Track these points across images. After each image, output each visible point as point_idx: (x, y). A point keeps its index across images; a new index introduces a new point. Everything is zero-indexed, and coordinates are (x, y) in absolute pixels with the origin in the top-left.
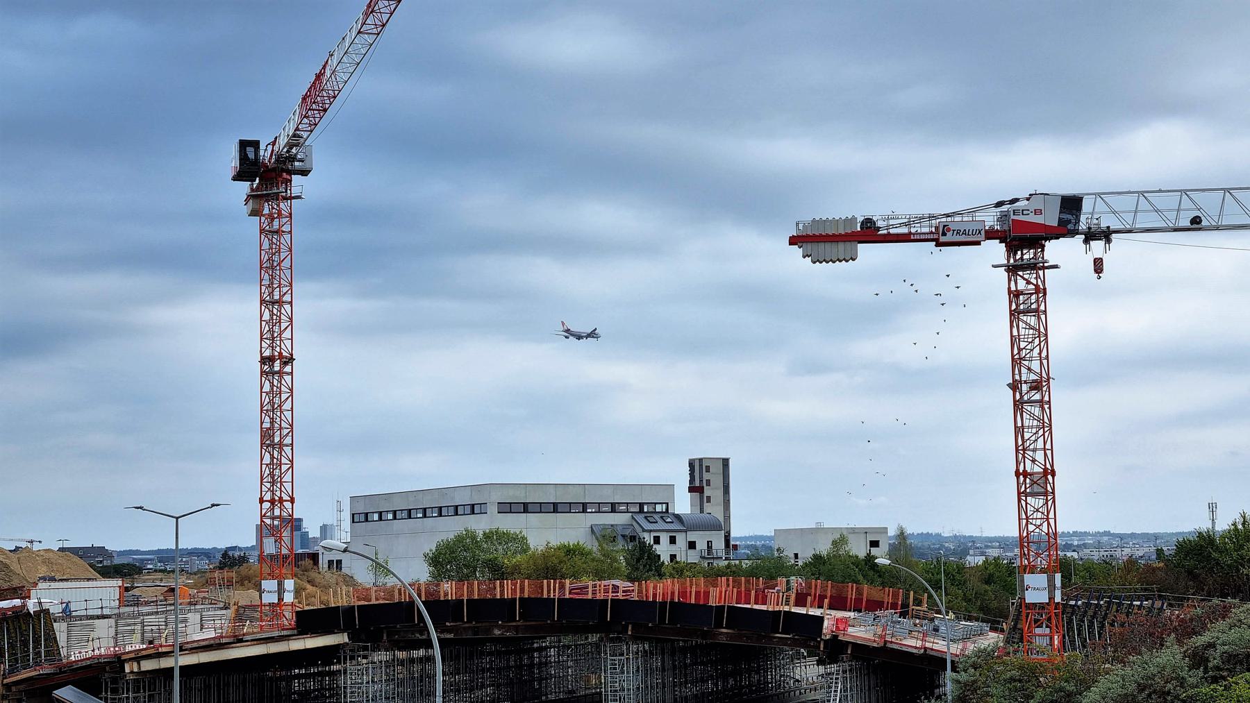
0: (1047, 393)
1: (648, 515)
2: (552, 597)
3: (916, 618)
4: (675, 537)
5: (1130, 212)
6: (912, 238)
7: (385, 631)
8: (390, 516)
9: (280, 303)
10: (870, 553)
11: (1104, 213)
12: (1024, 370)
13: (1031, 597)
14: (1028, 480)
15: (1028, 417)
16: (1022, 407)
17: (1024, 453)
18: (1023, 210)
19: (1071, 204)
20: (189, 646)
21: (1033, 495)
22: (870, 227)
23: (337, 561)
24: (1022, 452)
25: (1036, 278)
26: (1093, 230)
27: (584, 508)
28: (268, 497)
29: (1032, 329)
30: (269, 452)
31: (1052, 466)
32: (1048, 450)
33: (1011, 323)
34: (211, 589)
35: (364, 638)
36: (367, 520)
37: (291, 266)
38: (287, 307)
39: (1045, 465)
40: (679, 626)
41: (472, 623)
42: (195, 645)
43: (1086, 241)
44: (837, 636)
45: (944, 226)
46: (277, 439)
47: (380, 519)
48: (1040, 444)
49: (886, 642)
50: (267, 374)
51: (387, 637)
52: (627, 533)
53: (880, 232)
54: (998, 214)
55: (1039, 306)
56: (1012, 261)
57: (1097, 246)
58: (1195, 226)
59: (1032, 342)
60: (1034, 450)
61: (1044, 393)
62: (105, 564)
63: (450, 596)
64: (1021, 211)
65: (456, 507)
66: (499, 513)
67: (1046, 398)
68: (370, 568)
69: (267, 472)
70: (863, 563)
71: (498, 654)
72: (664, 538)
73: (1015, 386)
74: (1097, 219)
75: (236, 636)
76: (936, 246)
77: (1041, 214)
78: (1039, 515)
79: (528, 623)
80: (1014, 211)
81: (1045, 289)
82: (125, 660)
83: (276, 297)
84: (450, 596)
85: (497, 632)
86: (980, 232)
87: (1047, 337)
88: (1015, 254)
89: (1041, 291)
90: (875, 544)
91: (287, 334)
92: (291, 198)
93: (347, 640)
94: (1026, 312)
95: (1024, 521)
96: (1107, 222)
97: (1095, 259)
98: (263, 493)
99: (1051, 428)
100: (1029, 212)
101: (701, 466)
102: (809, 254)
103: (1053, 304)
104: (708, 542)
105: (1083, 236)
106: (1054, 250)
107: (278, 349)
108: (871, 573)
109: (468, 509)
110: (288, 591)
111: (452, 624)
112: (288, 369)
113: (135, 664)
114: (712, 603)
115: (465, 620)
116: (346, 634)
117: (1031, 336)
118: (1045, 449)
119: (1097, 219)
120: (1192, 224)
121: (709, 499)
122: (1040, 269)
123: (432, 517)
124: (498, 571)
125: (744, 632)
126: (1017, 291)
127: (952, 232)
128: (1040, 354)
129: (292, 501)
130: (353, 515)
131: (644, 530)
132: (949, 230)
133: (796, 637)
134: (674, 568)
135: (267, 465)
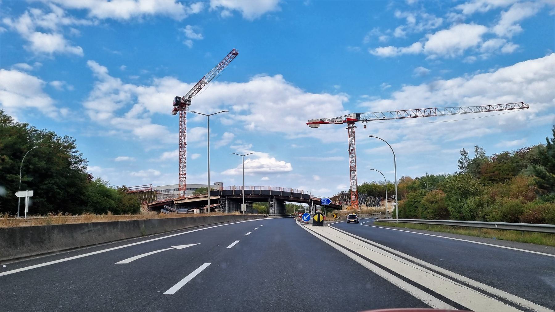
43: (363, 122)
57: (365, 123)
106: (357, 124)
113: (176, 202)
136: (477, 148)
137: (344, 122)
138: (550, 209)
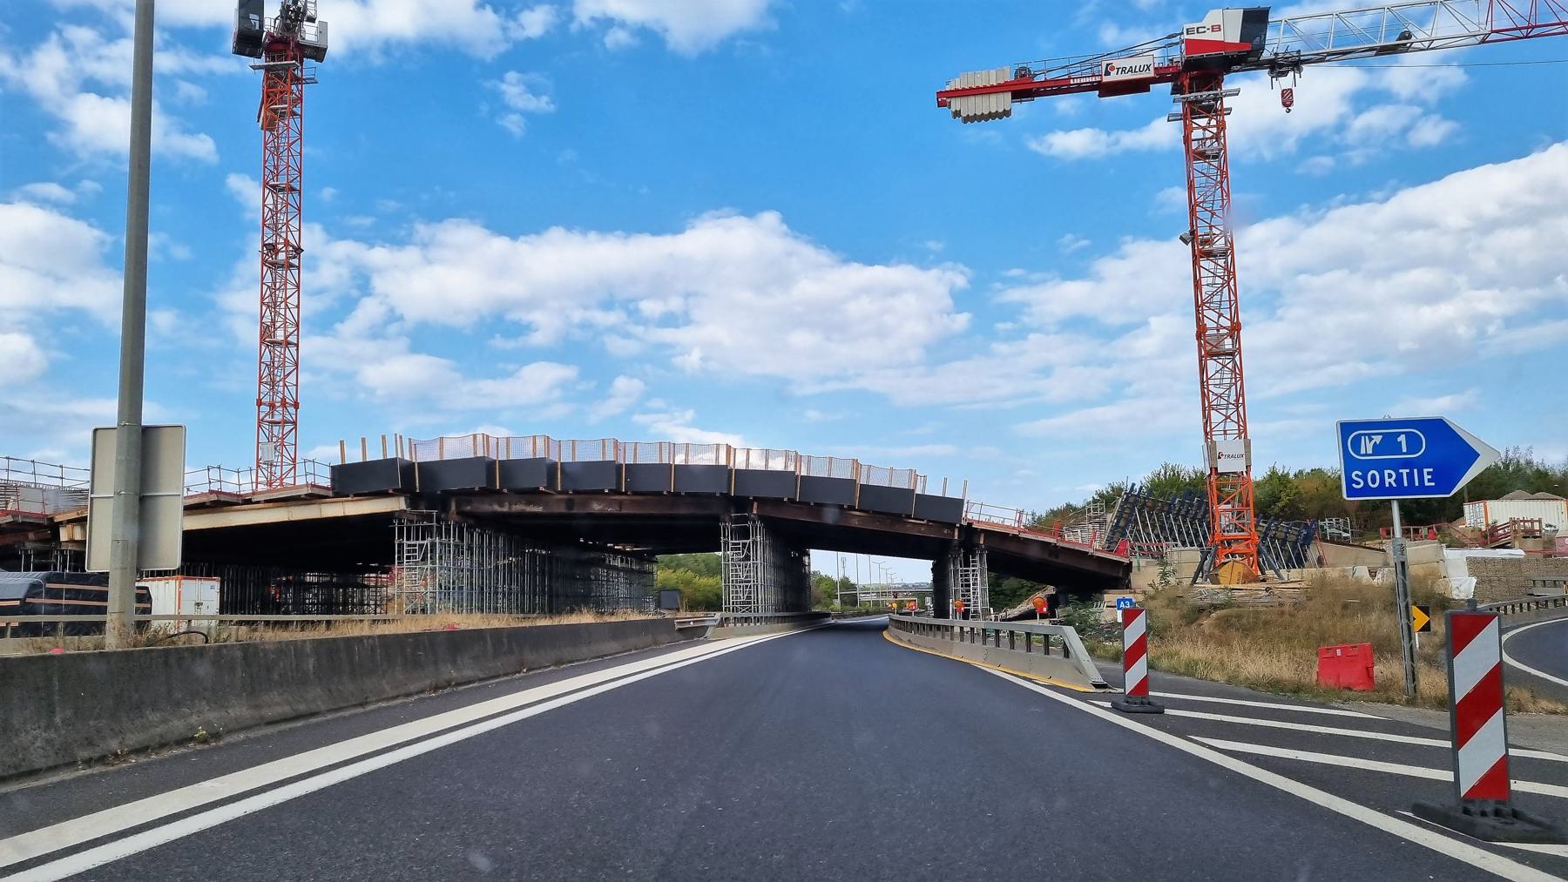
22: (1024, 75)
28: (266, 400)
51: (456, 508)
57: (1286, 82)
77: (1220, 30)
82: (61, 523)
86: (1148, 67)
91: (291, 379)
98: (262, 396)
129: (296, 405)
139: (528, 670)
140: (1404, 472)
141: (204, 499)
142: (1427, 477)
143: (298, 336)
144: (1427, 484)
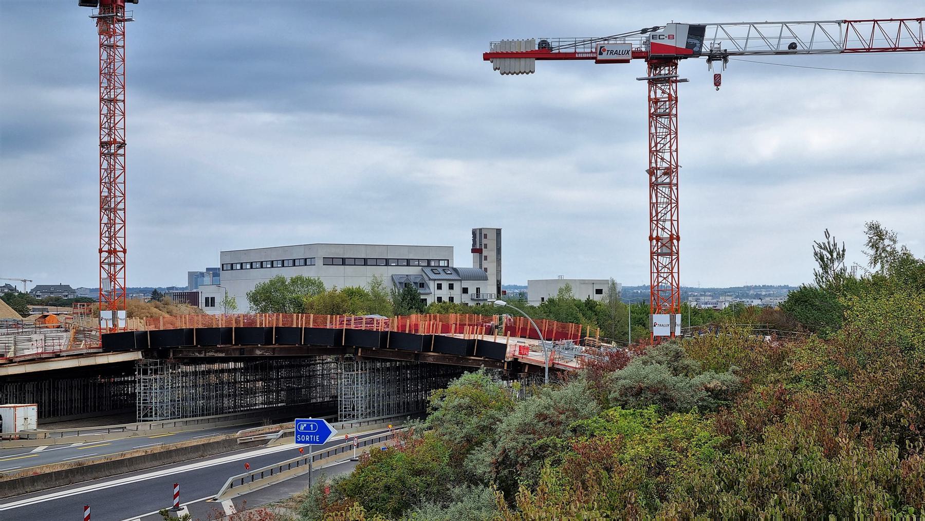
0: (676, 177)
1: (434, 268)
2: (300, 326)
3: (587, 345)
4: (441, 284)
5: (743, 38)
6: (577, 56)
7: (171, 351)
8: (248, 266)
9: (113, 101)
10: (589, 298)
11: (723, 39)
12: (659, 160)
13: (658, 331)
14: (659, 244)
15: (660, 195)
16: (657, 188)
17: (657, 223)
18: (659, 36)
19: (697, 31)
20: (18, 359)
21: (663, 254)
22: (545, 47)
23: (211, 298)
24: (655, 222)
25: (669, 89)
26: (714, 52)
27: (387, 262)
28: (106, 248)
29: (665, 128)
30: (108, 215)
31: (678, 233)
32: (675, 220)
33: (650, 123)
34: (75, 317)
35: (156, 356)
36: (232, 269)
37: (124, 73)
38: (121, 104)
39: (671, 232)
40: (396, 350)
41: (238, 345)
42: (22, 359)
43: (709, 61)
44: (517, 359)
45: (601, 47)
46: (113, 206)
47: (242, 268)
48: (668, 216)
49: (554, 364)
50: (105, 155)
51: (173, 355)
52: (418, 281)
53: (553, 52)
54: (645, 38)
55: (671, 111)
56: (652, 75)
57: (717, 65)
58: (792, 50)
59: (664, 138)
60: (664, 221)
61: (672, 178)
62: (69, 297)
63: (264, 324)
64: (658, 36)
65: (306, 260)
66: (324, 265)
67: (675, 181)
68: (222, 304)
69: (106, 229)
70: (584, 305)
71: (291, 366)
72: (445, 285)
73: (651, 172)
74: (719, 44)
75: (55, 352)
76: (596, 63)
77: (673, 39)
78: (666, 270)
79: (282, 346)
80: (653, 36)
81: (676, 98)
83: (112, 96)
84: (264, 324)
85: (258, 353)
86: (628, 52)
87: (677, 135)
88: (656, 70)
89: (673, 100)
90: (599, 292)
92: (125, 20)
93: (141, 357)
94: (661, 116)
95: (656, 275)
96: (727, 46)
97: (715, 75)
98: (102, 246)
99: (678, 204)
100: (664, 37)
101: (481, 233)
102: (498, 67)
103: (682, 109)
104: (477, 288)
105: (707, 57)
106: (685, 67)
107: (113, 137)
108: (589, 312)
109: (302, 262)
110: (121, 319)
111: (222, 346)
112: (121, 151)
114: (421, 332)
115: (234, 343)
116: (140, 352)
117: (664, 134)
118: (671, 220)
119: (719, 44)
120: (789, 49)
121: (486, 258)
122: (673, 82)
123: (277, 267)
124: (300, 307)
125: (447, 355)
126: (655, 98)
127: (606, 52)
128: (670, 147)
129: (125, 251)
130: (223, 265)
131: (430, 279)
132: (604, 50)
133: (486, 359)
134: (441, 307)
135: (105, 224)
136: (877, 234)
137: (634, 58)
138: (428, 500)
139: (73, 483)
140: (311, 436)
141: (35, 357)
142: (317, 438)
143: (125, 203)
144: (317, 441)
